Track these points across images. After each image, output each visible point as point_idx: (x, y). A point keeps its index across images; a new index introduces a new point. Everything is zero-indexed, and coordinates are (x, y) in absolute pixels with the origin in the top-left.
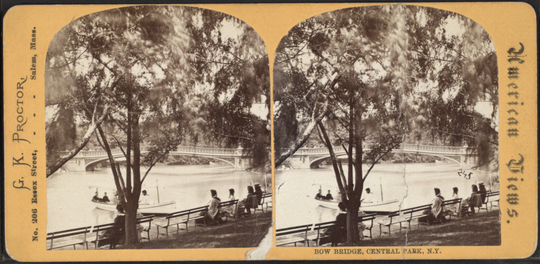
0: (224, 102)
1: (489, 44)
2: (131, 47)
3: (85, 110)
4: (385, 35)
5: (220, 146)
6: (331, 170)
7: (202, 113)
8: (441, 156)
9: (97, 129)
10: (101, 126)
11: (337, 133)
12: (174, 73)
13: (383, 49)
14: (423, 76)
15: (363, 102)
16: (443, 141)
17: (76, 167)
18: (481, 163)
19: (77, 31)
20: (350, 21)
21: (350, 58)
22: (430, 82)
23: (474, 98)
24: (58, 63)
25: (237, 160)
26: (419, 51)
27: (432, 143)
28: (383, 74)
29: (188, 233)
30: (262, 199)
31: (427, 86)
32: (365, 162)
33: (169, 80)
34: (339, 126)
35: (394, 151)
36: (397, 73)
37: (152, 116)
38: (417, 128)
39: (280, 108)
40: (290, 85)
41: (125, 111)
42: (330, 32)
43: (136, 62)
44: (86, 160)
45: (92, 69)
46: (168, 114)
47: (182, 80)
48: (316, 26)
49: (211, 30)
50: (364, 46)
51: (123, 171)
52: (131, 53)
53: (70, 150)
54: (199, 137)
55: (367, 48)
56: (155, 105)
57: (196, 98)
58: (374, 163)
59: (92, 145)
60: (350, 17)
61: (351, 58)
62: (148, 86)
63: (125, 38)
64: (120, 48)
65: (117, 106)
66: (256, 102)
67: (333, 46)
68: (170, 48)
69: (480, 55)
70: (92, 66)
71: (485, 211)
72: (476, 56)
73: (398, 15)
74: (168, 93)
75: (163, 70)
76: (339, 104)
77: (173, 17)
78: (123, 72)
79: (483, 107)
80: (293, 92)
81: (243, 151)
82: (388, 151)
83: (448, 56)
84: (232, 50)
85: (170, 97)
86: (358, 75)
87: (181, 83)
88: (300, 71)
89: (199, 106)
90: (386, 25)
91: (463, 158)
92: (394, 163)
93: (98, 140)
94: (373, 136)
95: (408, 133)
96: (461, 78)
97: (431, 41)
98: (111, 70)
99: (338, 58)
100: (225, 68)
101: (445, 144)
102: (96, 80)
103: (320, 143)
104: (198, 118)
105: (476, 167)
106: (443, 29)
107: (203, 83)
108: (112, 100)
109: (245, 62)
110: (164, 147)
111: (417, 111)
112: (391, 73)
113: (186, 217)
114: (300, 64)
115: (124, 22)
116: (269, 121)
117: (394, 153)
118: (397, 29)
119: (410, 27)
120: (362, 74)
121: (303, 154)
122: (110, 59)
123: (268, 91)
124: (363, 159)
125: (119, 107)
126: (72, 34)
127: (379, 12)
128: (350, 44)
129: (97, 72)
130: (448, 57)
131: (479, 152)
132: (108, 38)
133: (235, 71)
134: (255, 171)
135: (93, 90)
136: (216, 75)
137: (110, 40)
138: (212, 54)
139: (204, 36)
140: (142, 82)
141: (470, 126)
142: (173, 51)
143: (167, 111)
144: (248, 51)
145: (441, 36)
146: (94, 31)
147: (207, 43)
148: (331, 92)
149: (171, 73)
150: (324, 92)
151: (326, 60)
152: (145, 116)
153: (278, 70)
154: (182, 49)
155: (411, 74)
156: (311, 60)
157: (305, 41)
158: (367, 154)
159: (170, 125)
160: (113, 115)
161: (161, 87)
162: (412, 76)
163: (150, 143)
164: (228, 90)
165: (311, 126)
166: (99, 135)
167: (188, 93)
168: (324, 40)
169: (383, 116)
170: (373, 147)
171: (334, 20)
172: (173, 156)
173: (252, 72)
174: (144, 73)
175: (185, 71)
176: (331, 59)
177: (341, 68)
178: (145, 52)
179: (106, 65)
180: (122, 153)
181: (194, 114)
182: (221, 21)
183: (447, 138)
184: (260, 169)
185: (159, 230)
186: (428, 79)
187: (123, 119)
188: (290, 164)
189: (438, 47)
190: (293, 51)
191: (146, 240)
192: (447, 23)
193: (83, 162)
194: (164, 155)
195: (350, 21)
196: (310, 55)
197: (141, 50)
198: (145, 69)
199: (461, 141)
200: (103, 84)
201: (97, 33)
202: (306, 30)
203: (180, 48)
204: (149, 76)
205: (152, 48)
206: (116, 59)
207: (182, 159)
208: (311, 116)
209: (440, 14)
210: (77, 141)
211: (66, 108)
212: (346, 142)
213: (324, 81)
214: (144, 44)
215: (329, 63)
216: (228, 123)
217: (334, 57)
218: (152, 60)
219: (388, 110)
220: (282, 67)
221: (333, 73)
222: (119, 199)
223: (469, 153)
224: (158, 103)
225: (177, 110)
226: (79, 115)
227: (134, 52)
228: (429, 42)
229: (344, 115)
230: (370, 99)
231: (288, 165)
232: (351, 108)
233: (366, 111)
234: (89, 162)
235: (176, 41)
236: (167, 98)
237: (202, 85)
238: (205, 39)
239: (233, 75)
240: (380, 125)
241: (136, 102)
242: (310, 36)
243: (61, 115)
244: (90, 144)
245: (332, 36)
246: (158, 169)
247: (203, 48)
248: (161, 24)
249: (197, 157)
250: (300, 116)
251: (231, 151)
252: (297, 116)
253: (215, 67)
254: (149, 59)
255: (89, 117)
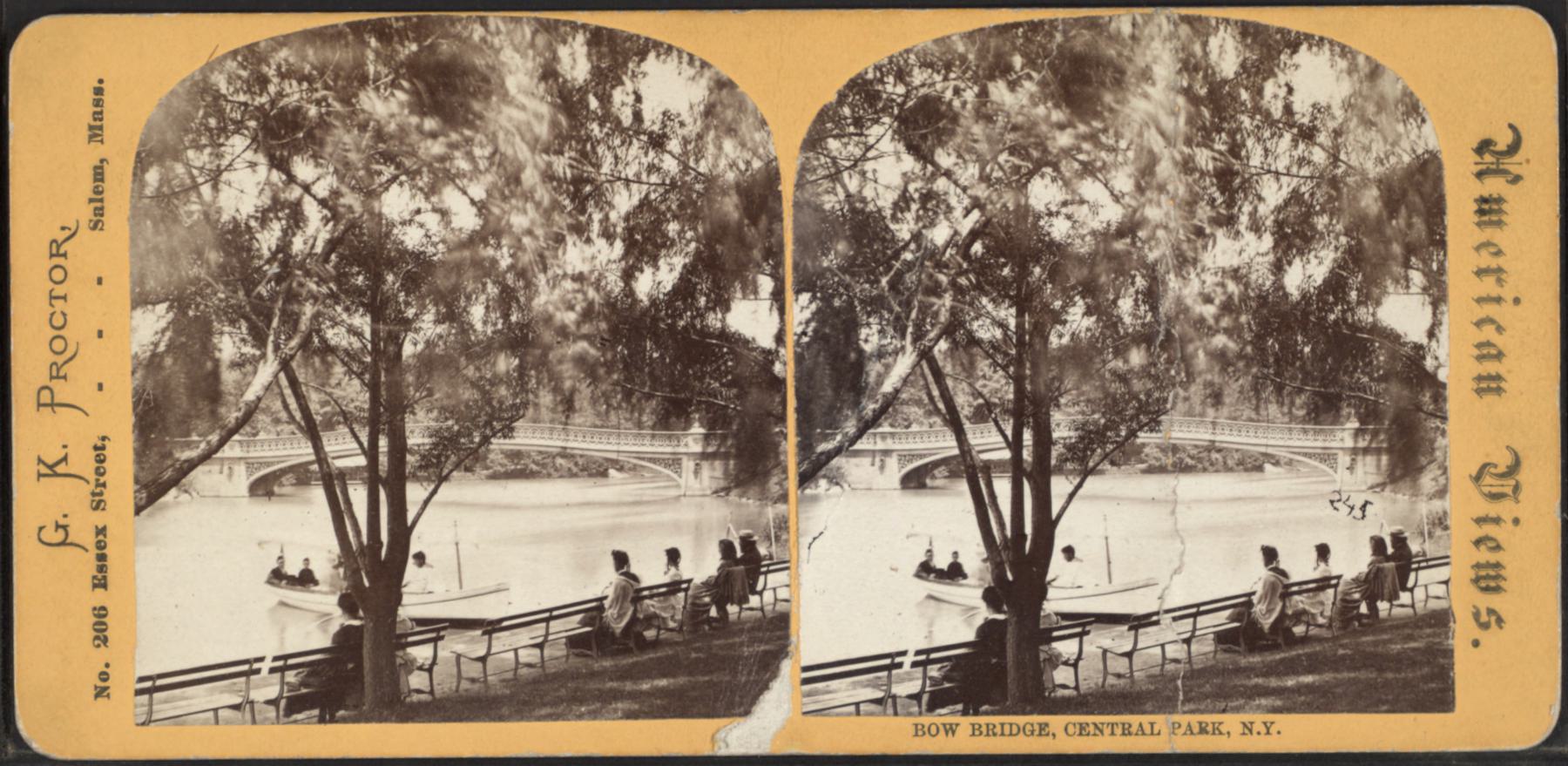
0: (650, 297)
1: (1419, 128)
2: (379, 135)
3: (248, 319)
4: (1118, 102)
5: (640, 425)
6: (960, 494)
7: (586, 329)
8: (1282, 454)
9: (282, 375)
10: (294, 364)
11: (978, 385)
12: (504, 212)
13: (1111, 142)
14: (1228, 221)
15: (1054, 296)
16: (1286, 409)
17: (221, 484)
18: (1398, 473)
19: (224, 91)
20: (1018, 61)
21: (1016, 169)
22: (1250, 237)
23: (1377, 285)
24: (169, 182)
25: (688, 465)
26: (1217, 147)
27: (1253, 415)
28: (1113, 214)
29: (546, 676)
30: (762, 579)
31: (1241, 251)
32: (1060, 470)
33: (490, 232)
34: (983, 366)
35: (1143, 437)
36: (1153, 213)
37: (440, 337)
38: (1210, 370)
39: (814, 314)
40: (841, 246)
41: (362, 322)
42: (957, 92)
43: (394, 179)
44: (251, 465)
45: (266, 200)
46: (489, 332)
47: (529, 232)
48: (918, 77)
49: (613, 87)
50: (1057, 134)
51: (358, 496)
52: (381, 154)
53: (203, 435)
54: (577, 397)
55: (1064, 139)
56: (449, 306)
57: (568, 285)
58: (1086, 473)
59: (268, 420)
60: (1015, 49)
61: (1020, 167)
62: (431, 250)
63: (363, 111)
64: (347, 139)
65: (339, 309)
66: (744, 297)
67: (968, 133)
68: (493, 139)
69: (1393, 160)
70: (268, 193)
71: (1409, 611)
72: (1381, 162)
73: (1156, 44)
74: (487, 269)
75: (473, 202)
76: (984, 301)
77: (501, 48)
78: (358, 208)
79: (1401, 312)
80: (849, 267)
81: (707, 438)
82: (1127, 438)
83: (1302, 162)
84: (674, 145)
85: (494, 283)
86: (1038, 217)
87: (526, 240)
88: (871, 207)
89: (578, 308)
90: (1122, 72)
91: (1344, 460)
92: (1145, 472)
93: (286, 406)
94: (1083, 394)
95: (1185, 385)
96: (1339, 227)
97: (1252, 118)
98: (323, 203)
99: (982, 169)
100: (653, 196)
101: (1293, 418)
102: (278, 233)
103: (929, 414)
104: (574, 341)
105: (1383, 485)
106: (1287, 85)
107: (589, 241)
108: (324, 290)
109: (710, 180)
110: (478, 427)
111: (1211, 321)
112: (1135, 211)
113: (540, 629)
114: (871, 185)
115: (360, 64)
116: (782, 351)
117: (1144, 445)
118: (1154, 84)
119: (1192, 79)
120: (1050, 214)
121: (880, 445)
122: (320, 171)
123: (779, 264)
124: (1053, 462)
125: (347, 309)
126: (209, 99)
127: (1100, 34)
128: (1015, 128)
129: (282, 209)
130: (1300, 166)
131: (1390, 440)
132: (313, 111)
133: (681, 206)
134: (741, 496)
135: (269, 262)
136: (627, 219)
137: (321, 115)
138: (616, 157)
139: (594, 103)
140: (412, 238)
141: (1366, 365)
142: (502, 147)
143: (485, 323)
144: (720, 148)
145: (1280, 104)
146: (272, 89)
147: (601, 125)
148: (960, 266)
149: (496, 211)
150: (940, 266)
151: (948, 174)
152: (421, 338)
153: (808, 203)
154: (528, 143)
155: (1192, 213)
156: (904, 174)
157: (887, 120)
158: (1065, 446)
159: (494, 364)
160: (330, 334)
161: (467, 253)
162: (1196, 222)
163: (435, 413)
164: (661, 262)
165: (903, 364)
166: (288, 392)
167: (545, 270)
168: (942, 116)
169: (1113, 336)
170: (435, 433)
171: (971, 57)
172: (502, 452)
173: (731, 208)
174: (418, 212)
175: (538, 205)
176: (961, 172)
177: (989, 197)
178: (421, 152)
179: (307, 188)
180: (355, 445)
181: (563, 332)
182: (642, 60)
183: (1298, 401)
184: (754, 490)
185: (463, 667)
186: (1242, 228)
187: (357, 344)
188: (843, 476)
189: (1273, 136)
190: (850, 148)
191: (423, 697)
192: (1297, 67)
193: (240, 469)
194: (476, 450)
195: (1018, 61)
196: (899, 159)
197: (410, 145)
198: (420, 202)
199: (1338, 410)
200: (298, 245)
201: (280, 95)
202: (889, 88)
203: (523, 139)
204: (432, 221)
205: (441, 139)
206: (336, 171)
207: (1182, 455)
208: (903, 337)
209: (1277, 42)
210: (223, 410)
211: (191, 313)
212: (1006, 411)
213: (939, 234)
214: (419, 129)
215: (956, 183)
216: (662, 357)
217: (971, 165)
218: (442, 175)
219: (1127, 320)
220: (819, 195)
221: (967, 212)
222: (345, 578)
223: (1362, 444)
224: (458, 299)
225: (514, 318)
226: (230, 334)
227: (390, 152)
228: (1246, 121)
229: (998, 333)
230: (1073, 288)
231: (835, 480)
232: (1020, 315)
233: (1064, 323)
234: (910, 461)
235: (510, 119)
236: (484, 285)
237: (586, 247)
238: (594, 112)
239: (675, 217)
240: (1105, 362)
241: (396, 296)
242: (901, 106)
243: (177, 332)
244: (262, 419)
245: (964, 104)
246: (459, 489)
247: (589, 138)
248: (468, 71)
249: (573, 456)
250: (870, 337)
251: (670, 437)
252: (863, 336)
253: (625, 193)
254: (432, 171)
255: (259, 338)
